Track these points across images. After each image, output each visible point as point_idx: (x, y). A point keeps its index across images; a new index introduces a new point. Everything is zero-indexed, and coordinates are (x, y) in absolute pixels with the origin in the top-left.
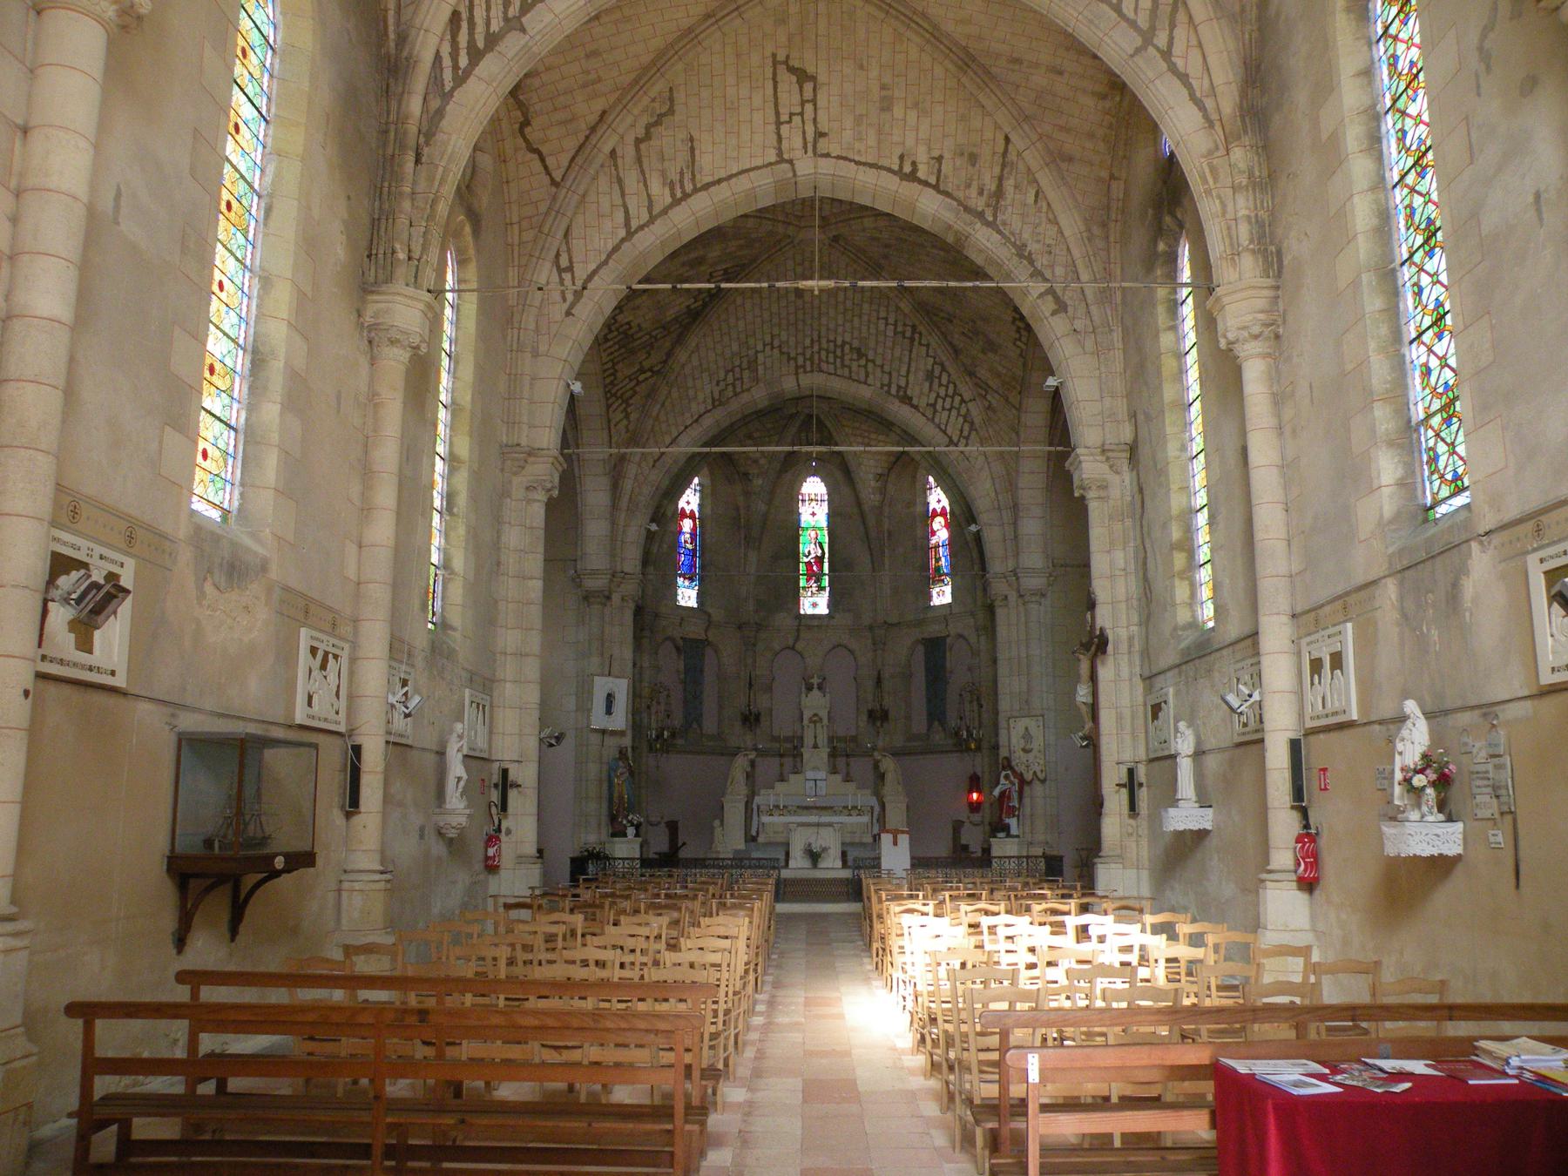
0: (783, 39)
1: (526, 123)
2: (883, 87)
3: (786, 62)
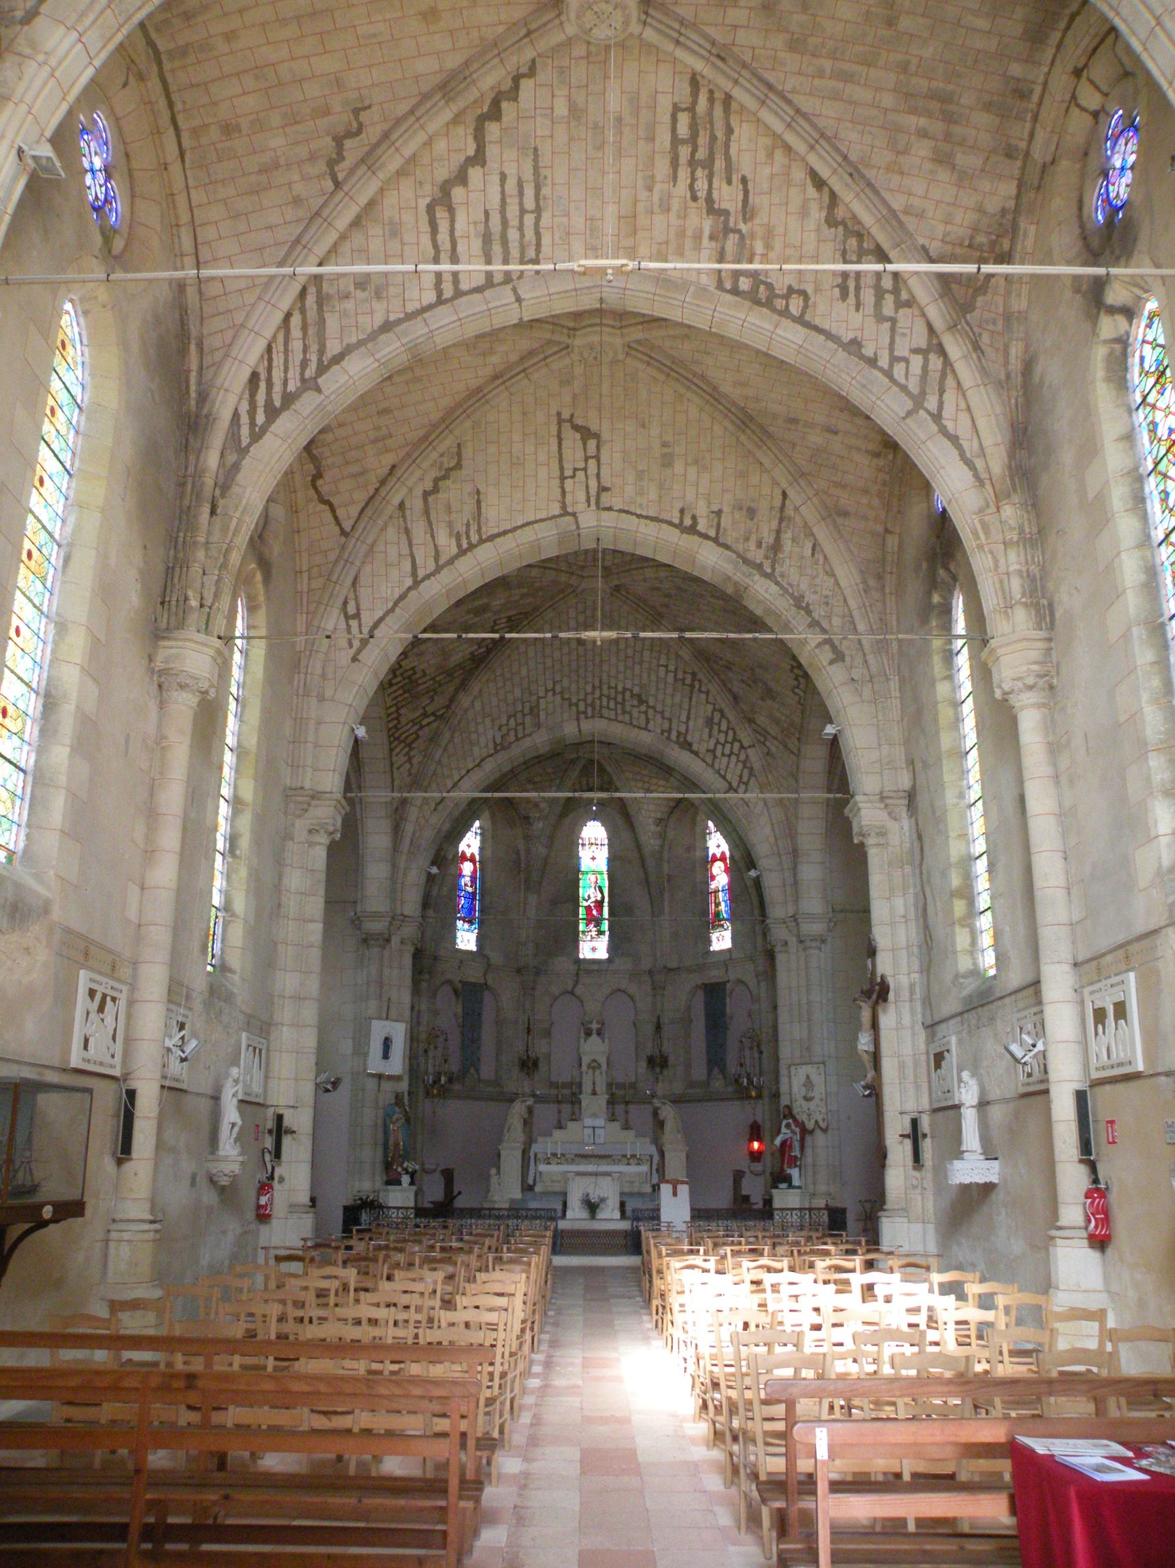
0: (567, 398)
1: (318, 475)
2: (665, 445)
3: (571, 420)
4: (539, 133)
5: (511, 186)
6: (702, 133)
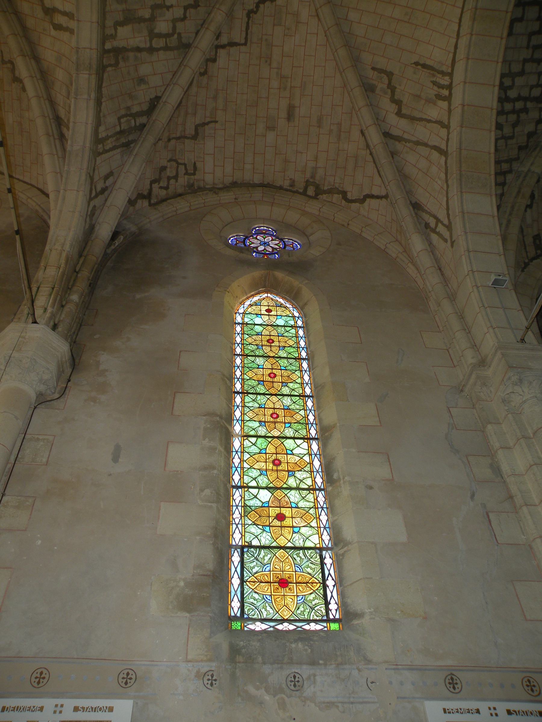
1: (344, 194)
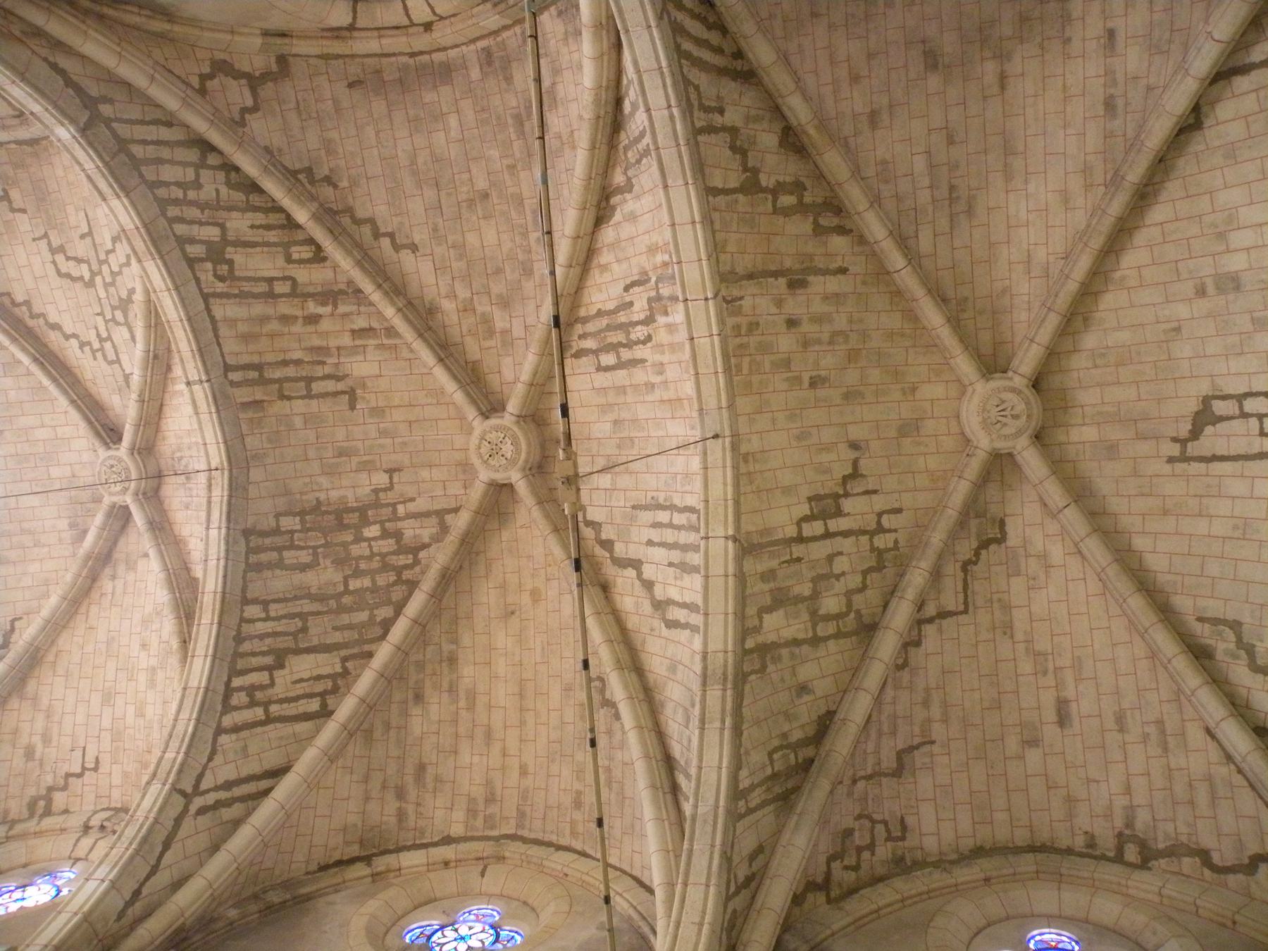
0: (1145, 448)
2: (1201, 292)
3: (1183, 442)
4: (622, 504)
5: (655, 535)
6: (609, 340)
